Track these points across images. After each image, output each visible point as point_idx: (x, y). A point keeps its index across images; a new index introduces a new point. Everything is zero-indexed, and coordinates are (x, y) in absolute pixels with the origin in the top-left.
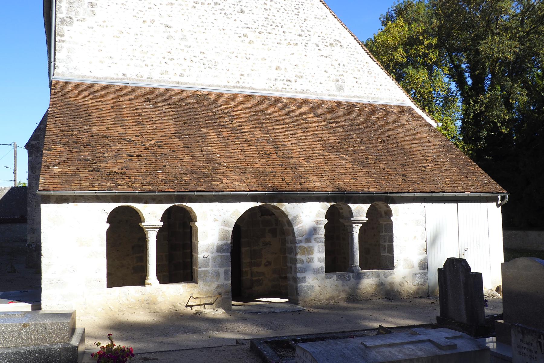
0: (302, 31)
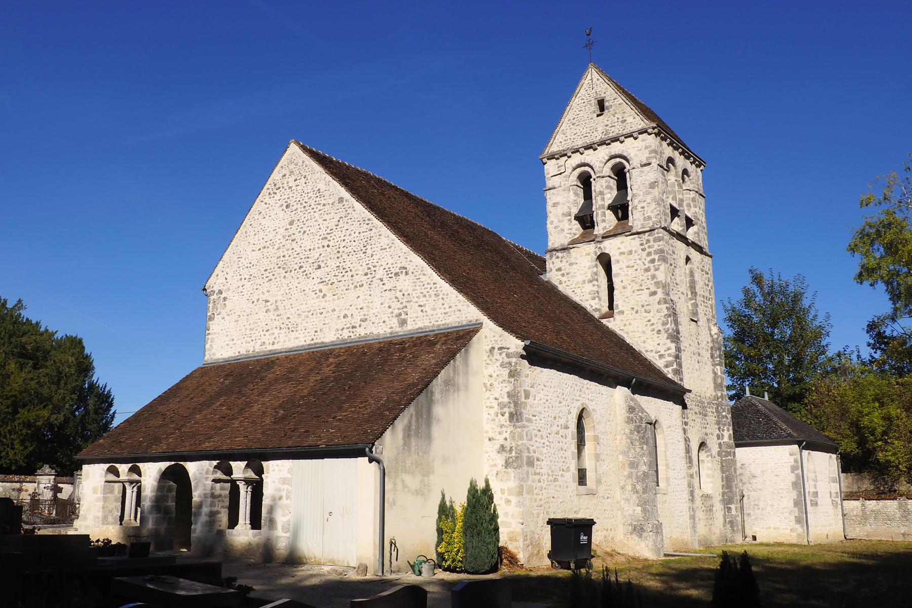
0: (369, 268)
